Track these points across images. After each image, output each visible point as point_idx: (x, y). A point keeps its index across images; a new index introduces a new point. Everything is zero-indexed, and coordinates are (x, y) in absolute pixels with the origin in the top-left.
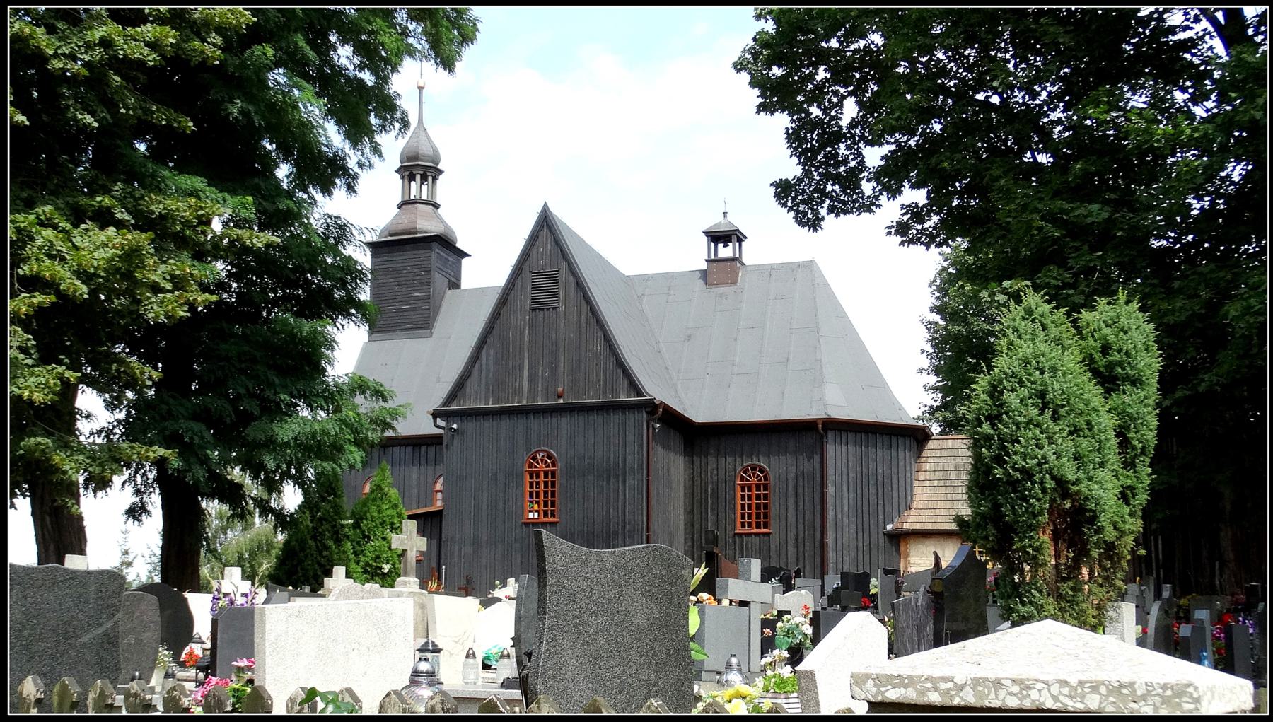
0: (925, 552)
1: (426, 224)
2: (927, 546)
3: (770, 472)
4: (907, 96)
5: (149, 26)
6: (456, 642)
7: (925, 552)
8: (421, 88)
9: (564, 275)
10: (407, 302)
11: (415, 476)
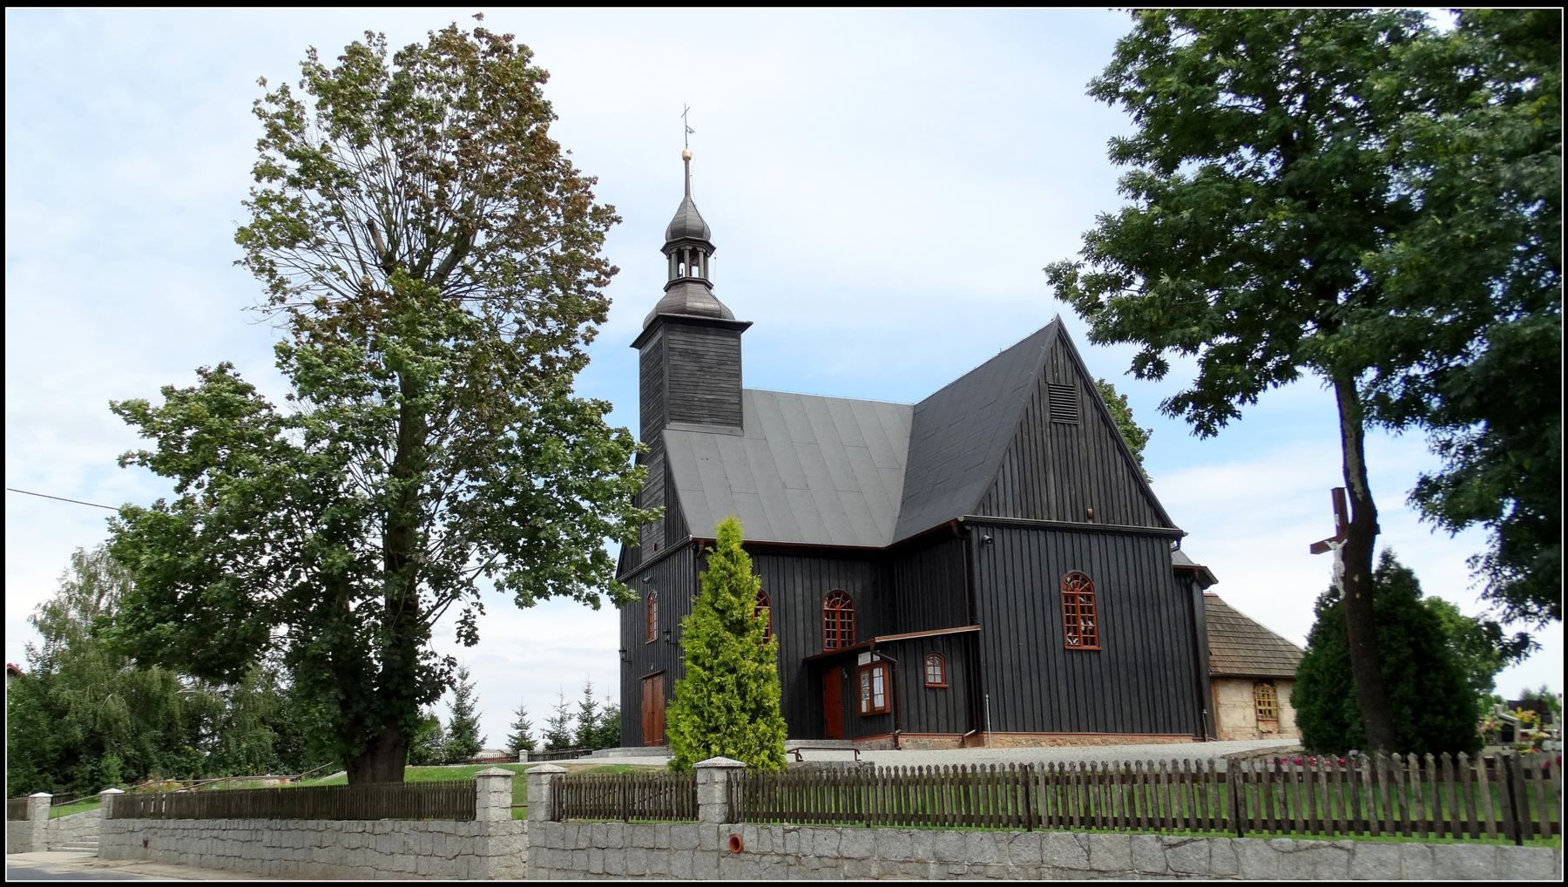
1: (696, 301)
5: (1524, 105)
6: (481, 606)
8: (687, 159)
9: (1080, 393)
10: (711, 392)
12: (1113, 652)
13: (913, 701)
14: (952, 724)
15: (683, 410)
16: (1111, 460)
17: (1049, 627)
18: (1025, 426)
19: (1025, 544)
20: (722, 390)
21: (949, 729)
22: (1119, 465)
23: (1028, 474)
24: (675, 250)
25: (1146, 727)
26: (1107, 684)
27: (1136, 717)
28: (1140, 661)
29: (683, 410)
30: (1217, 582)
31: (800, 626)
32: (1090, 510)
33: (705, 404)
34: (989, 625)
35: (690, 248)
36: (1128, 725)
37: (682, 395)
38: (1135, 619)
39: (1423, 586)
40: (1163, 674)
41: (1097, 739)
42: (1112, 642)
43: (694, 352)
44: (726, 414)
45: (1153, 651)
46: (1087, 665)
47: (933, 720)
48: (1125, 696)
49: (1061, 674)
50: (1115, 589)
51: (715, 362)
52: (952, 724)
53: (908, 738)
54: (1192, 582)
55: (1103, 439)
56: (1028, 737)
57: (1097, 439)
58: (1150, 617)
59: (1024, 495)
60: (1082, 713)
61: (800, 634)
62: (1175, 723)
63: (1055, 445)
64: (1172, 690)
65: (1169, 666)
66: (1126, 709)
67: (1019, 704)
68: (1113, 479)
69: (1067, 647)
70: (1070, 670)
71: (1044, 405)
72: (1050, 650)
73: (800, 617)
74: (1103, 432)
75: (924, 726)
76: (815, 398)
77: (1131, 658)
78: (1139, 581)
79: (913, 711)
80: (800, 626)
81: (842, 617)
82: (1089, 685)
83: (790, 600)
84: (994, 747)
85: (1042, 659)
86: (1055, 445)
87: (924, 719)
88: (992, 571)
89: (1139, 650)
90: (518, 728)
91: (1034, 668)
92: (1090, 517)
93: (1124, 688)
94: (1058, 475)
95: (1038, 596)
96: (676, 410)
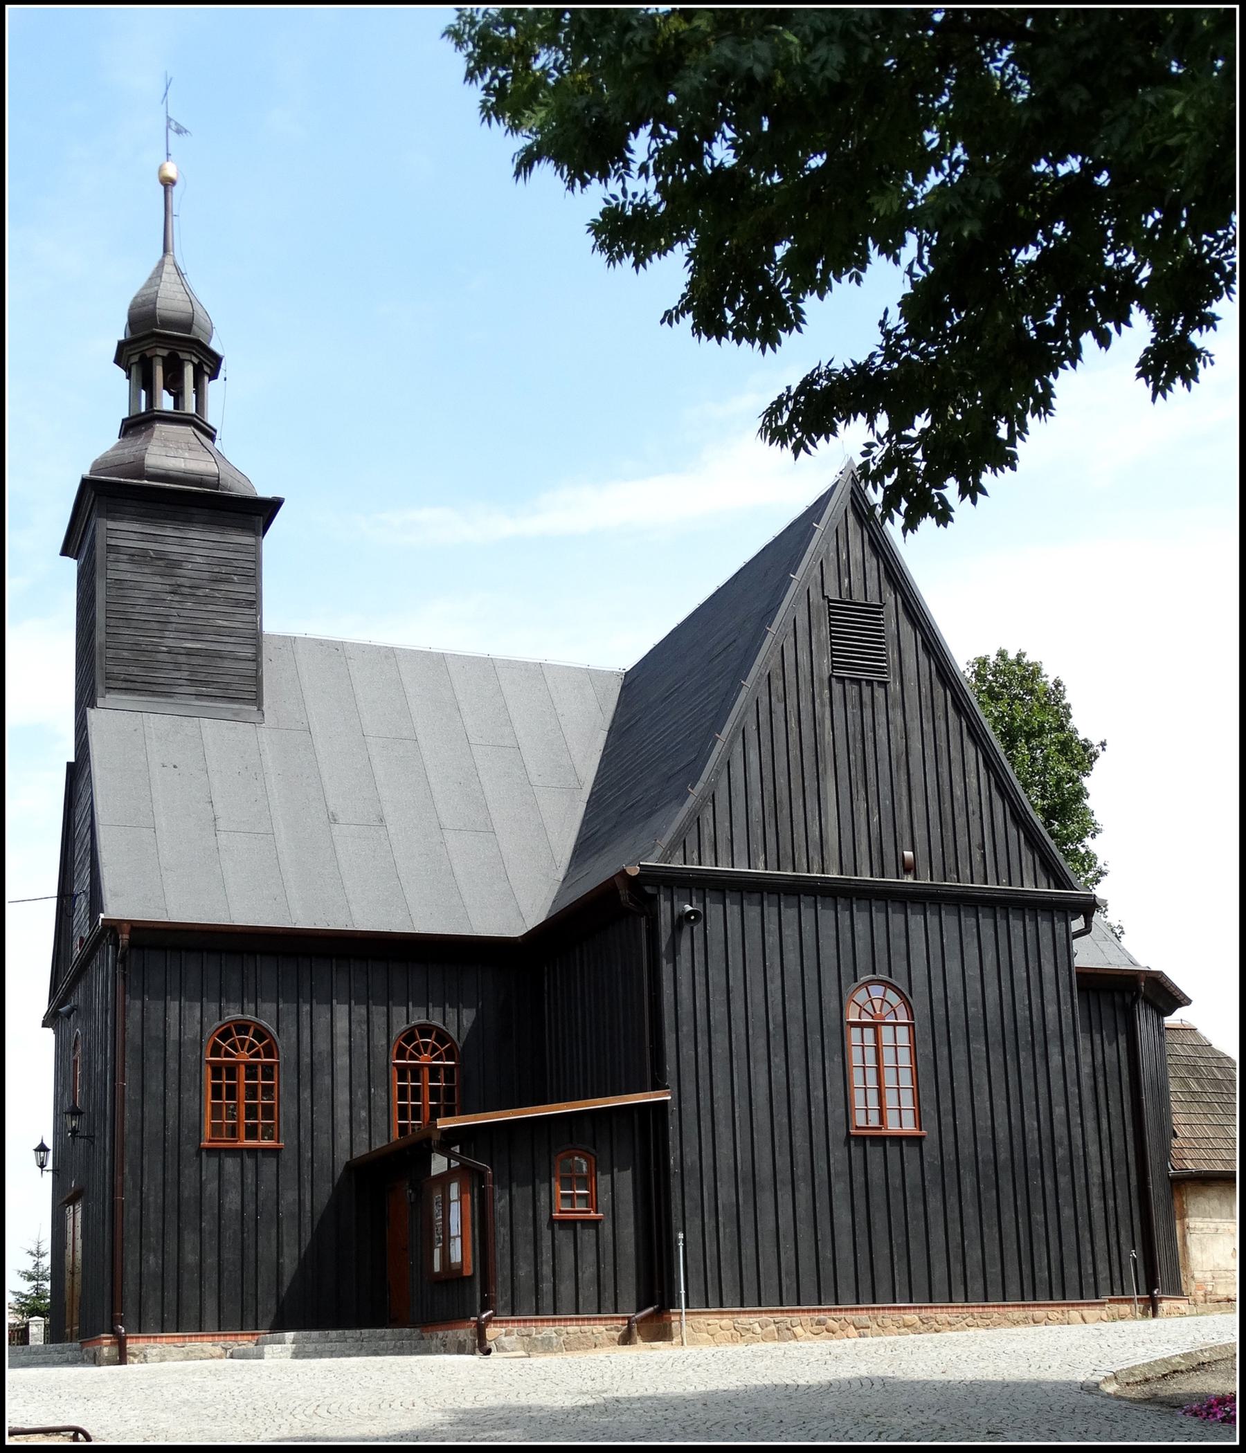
0: (1207, 1208)
2: (1209, 1200)
3: (278, 1040)
4: (1105, 174)
7: (1207, 1208)
8: (168, 183)
9: (892, 619)
10: (196, 634)
11: (342, 1025)
12: (949, 1138)
13: (525, 1250)
14: (608, 1294)
15: (136, 671)
16: (955, 754)
17: (818, 1094)
18: (777, 684)
19: (772, 926)
20: (220, 632)
21: (601, 1306)
22: (971, 766)
23: (782, 781)
24: (135, 359)
25: (1013, 1288)
26: (935, 1203)
27: (994, 1270)
28: (1003, 1155)
29: (136, 671)
30: (1188, 1002)
31: (343, 1096)
32: (908, 854)
33: (182, 659)
34: (689, 1087)
35: (165, 353)
36: (976, 1286)
37: (132, 640)
38: (997, 1070)
39: (1092, 337)
40: (1049, 1183)
41: (911, 1317)
42: (947, 1120)
43: (161, 556)
44: (227, 679)
45: (1032, 1136)
46: (894, 1166)
47: (566, 1288)
48: (972, 1229)
49: (840, 1187)
50: (956, 1013)
51: (206, 575)
52: (608, 1294)
53: (510, 1327)
54: (1135, 1001)
55: (940, 713)
56: (765, 1317)
57: (927, 713)
58: (1026, 1066)
59: (770, 821)
60: (882, 1267)
61: (342, 1113)
62: (1073, 1282)
63: (839, 724)
64: (1067, 1213)
65: (1063, 1165)
66: (974, 1255)
67: (749, 1251)
68: (958, 792)
69: (853, 1131)
70: (859, 1179)
71: (819, 640)
72: (819, 1138)
73: (342, 1077)
74: (940, 702)
75: (547, 1300)
76: (428, 655)
77: (985, 1152)
78: (1007, 998)
79: (524, 1270)
80: (343, 1096)
81: (434, 1078)
82: (897, 1208)
83: (322, 1045)
84: (694, 1342)
85: (802, 1157)
86: (839, 724)
87: (546, 1286)
88: (700, 979)
89: (1002, 1134)
90: (31, 1278)
91: (784, 1175)
92: (909, 868)
93: (970, 1211)
94: (844, 784)
95: (795, 1030)
96: (116, 669)
